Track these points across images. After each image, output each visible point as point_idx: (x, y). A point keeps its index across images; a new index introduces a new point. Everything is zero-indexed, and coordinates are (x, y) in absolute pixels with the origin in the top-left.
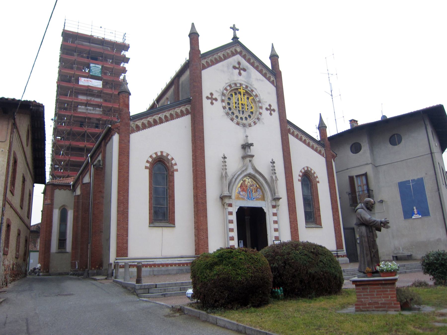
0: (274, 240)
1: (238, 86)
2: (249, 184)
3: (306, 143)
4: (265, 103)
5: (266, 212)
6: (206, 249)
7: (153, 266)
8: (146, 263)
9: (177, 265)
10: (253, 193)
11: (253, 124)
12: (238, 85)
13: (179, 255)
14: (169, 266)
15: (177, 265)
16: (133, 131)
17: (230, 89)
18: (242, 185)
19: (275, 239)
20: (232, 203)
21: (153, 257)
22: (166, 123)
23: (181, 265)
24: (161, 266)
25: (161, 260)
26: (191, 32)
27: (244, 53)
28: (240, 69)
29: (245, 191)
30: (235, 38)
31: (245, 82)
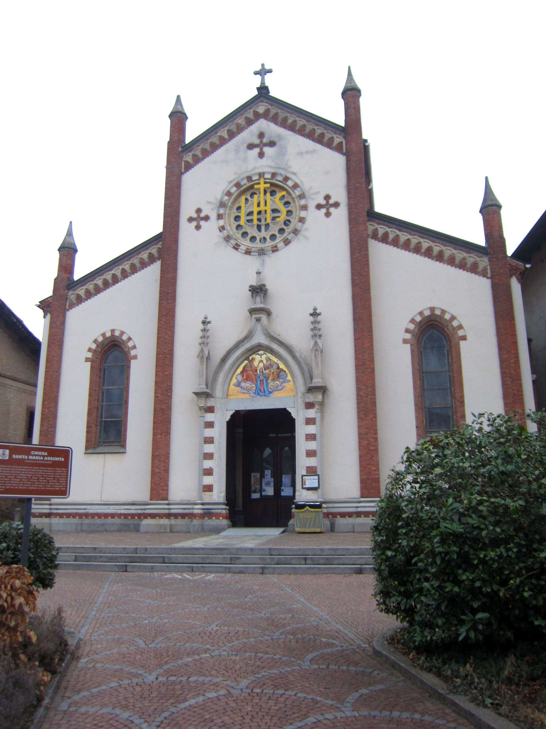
0: (305, 473)
1: (255, 180)
2: (261, 365)
3: (432, 254)
4: (313, 196)
5: (294, 417)
6: (163, 490)
7: (84, 517)
8: (74, 511)
9: (122, 517)
10: (269, 381)
11: (283, 244)
12: (255, 178)
13: (130, 499)
14: (110, 518)
15: (122, 517)
16: (72, 306)
17: (237, 190)
18: (247, 369)
19: (307, 472)
20: (214, 405)
21: (86, 502)
22: (123, 281)
23: (130, 517)
24: (96, 517)
25: (97, 507)
26: (175, 110)
27: (273, 111)
28: (261, 145)
29: (252, 381)
30: (263, 90)
31: (270, 167)
